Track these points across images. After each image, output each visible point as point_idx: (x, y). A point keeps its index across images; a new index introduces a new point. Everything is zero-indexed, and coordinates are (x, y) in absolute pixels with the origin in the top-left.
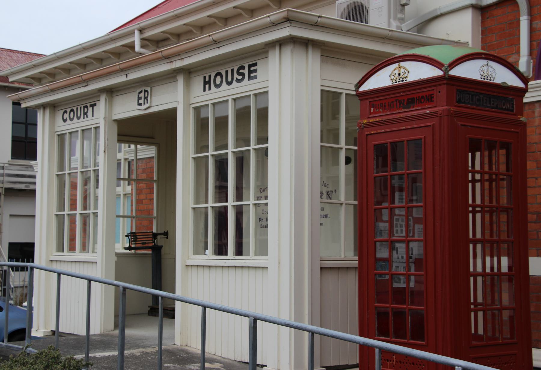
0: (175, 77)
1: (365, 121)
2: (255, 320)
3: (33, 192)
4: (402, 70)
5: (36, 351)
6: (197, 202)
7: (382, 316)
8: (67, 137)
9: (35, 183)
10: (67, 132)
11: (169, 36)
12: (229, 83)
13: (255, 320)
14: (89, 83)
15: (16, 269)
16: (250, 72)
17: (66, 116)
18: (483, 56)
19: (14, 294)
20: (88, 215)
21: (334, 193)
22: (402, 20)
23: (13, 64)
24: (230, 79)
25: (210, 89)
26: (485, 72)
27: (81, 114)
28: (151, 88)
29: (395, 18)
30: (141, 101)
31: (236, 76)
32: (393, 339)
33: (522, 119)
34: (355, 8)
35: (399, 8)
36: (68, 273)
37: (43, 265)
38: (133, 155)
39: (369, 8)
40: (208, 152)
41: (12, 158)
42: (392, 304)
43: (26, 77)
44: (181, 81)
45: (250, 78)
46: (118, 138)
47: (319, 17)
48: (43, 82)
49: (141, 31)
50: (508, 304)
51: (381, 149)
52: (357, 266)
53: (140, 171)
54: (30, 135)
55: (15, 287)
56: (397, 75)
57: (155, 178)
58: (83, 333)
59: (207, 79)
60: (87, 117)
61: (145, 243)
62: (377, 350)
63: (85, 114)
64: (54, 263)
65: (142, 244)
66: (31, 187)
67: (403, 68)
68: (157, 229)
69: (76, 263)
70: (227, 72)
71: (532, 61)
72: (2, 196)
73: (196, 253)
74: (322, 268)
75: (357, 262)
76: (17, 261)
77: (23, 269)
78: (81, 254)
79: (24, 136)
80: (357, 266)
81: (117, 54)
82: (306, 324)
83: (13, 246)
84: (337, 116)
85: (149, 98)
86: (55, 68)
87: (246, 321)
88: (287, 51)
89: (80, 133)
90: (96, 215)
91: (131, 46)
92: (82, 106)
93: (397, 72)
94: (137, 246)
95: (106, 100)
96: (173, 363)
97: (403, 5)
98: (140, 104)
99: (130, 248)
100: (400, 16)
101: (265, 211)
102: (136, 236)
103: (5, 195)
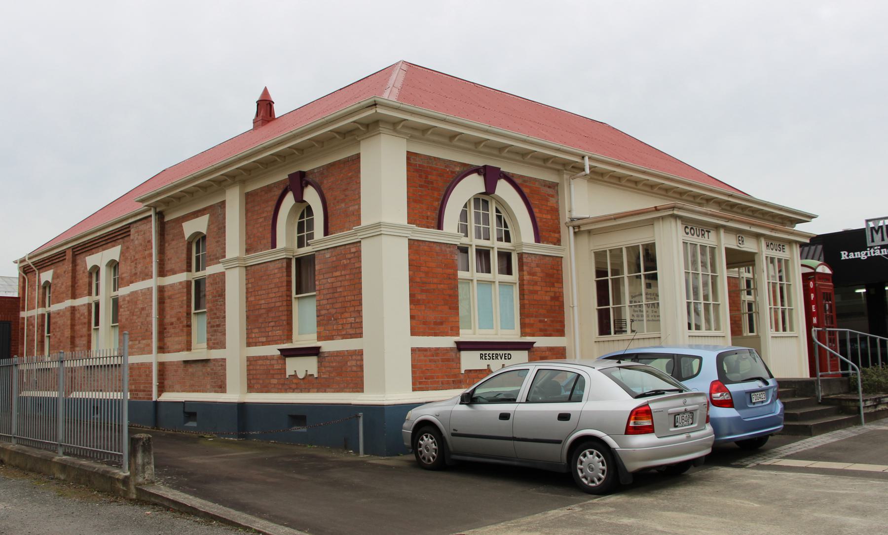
17: (688, 230)
30: (741, 242)
50: (808, 376)
60: (704, 238)
63: (703, 235)
92: (700, 229)
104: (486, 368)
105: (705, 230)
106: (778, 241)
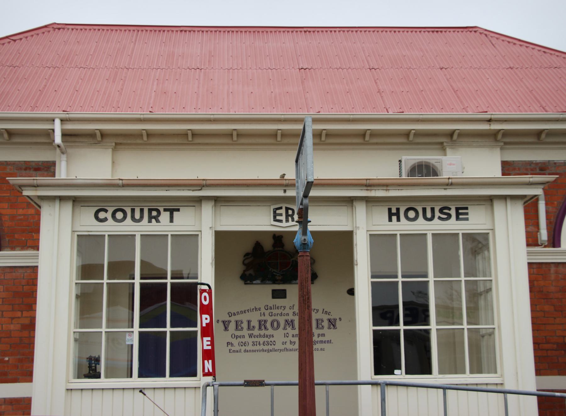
10: (170, 234)
14: (203, 188)
21: (338, 320)
39: (442, 169)
69: (407, 388)
84: (268, 245)
101: (236, 335)
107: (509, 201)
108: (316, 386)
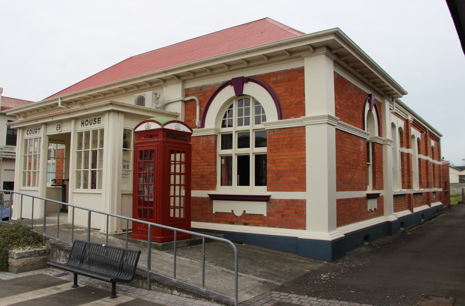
0: (71, 120)
1: (136, 142)
2: (90, 211)
3: (15, 159)
4: (149, 125)
5: (13, 223)
6: (78, 168)
7: (140, 211)
8: (28, 141)
9: (15, 156)
10: (28, 139)
11: (73, 101)
12: (91, 124)
13: (90, 211)
14: (38, 120)
15: (6, 193)
16: (98, 121)
17: (28, 132)
18: (176, 122)
19: (5, 204)
20: (35, 172)
22: (157, 103)
23: (9, 104)
24: (91, 123)
25: (84, 126)
26: (177, 127)
27: (34, 132)
28: (62, 124)
29: (154, 103)
31: (93, 122)
32: (143, 219)
33: (190, 143)
34: (141, 98)
35: (156, 99)
36: (26, 195)
37: (17, 191)
38: (56, 147)
40: (82, 149)
41: (6, 145)
42: (143, 207)
43: (14, 114)
44: (73, 122)
45: (98, 123)
46: (49, 141)
47: (123, 103)
48: (21, 116)
49: (61, 99)
51: (141, 152)
52: (132, 193)
53: (59, 154)
54: (14, 134)
55: (6, 201)
56: (147, 127)
57: (64, 157)
58: (31, 218)
59: (83, 122)
60: (37, 133)
61: (59, 184)
62: (175, 232)
63: (36, 132)
64: (22, 191)
65: (58, 184)
66: (14, 157)
67: (149, 124)
68: (65, 178)
70: (90, 120)
71: (200, 121)
72: (1, 161)
73: (77, 188)
74: (122, 194)
75: (132, 192)
76: (7, 190)
77: (9, 193)
78: (32, 187)
79: (12, 134)
80: (132, 193)
81: (52, 106)
82: (115, 215)
83: (5, 183)
85: (61, 128)
86: (26, 111)
87: (87, 212)
88: (111, 114)
89: (33, 140)
90: (38, 172)
91: (57, 104)
92: (35, 129)
93: (147, 125)
94: (56, 184)
95: (44, 127)
96: (66, 229)
97: (158, 98)
98: (57, 130)
99: (53, 185)
100: (156, 102)
102: (56, 180)
103: (2, 161)
104: (231, 212)
105: (37, 129)
106: (93, 116)
107: (120, 114)
108: (34, 218)
